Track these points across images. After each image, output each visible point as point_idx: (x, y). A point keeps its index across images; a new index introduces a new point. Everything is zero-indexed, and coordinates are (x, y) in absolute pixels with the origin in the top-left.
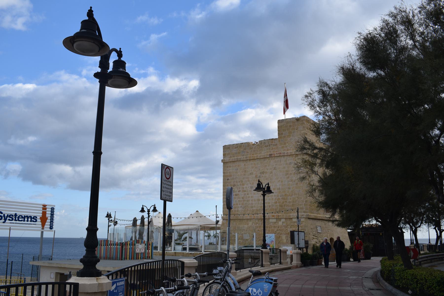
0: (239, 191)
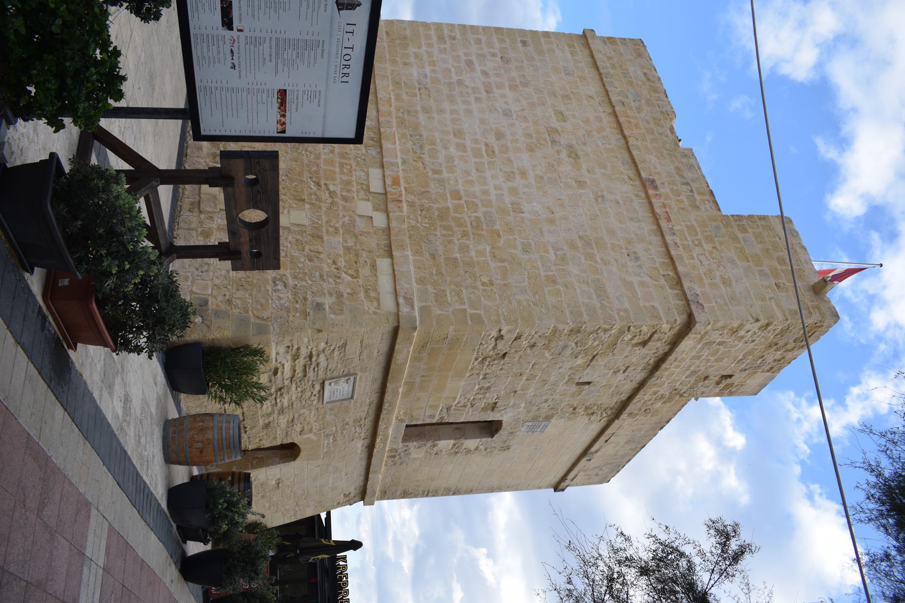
0: (485, 73)
